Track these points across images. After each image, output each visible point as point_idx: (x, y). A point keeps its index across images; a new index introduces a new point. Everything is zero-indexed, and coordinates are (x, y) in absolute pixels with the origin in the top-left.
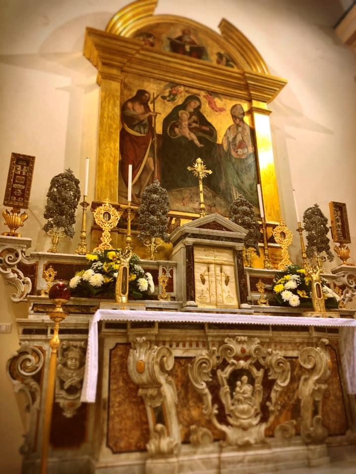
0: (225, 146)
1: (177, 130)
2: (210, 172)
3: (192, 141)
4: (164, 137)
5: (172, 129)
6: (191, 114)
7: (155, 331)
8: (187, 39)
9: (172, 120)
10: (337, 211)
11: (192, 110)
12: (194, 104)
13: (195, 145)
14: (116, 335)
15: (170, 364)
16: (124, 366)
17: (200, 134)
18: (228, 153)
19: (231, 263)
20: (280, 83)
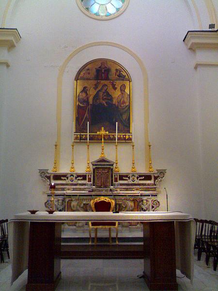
0: (117, 104)
1: (98, 101)
2: (103, 128)
3: (104, 104)
4: (93, 105)
5: (96, 101)
6: (104, 93)
7: (78, 197)
8: (103, 67)
9: (96, 97)
10: (116, 168)
11: (104, 91)
12: (105, 88)
13: (105, 106)
14: (69, 198)
15: (82, 205)
16: (70, 206)
17: (106, 101)
18: (117, 107)
19: (215, 36)
20: (62, 221)
